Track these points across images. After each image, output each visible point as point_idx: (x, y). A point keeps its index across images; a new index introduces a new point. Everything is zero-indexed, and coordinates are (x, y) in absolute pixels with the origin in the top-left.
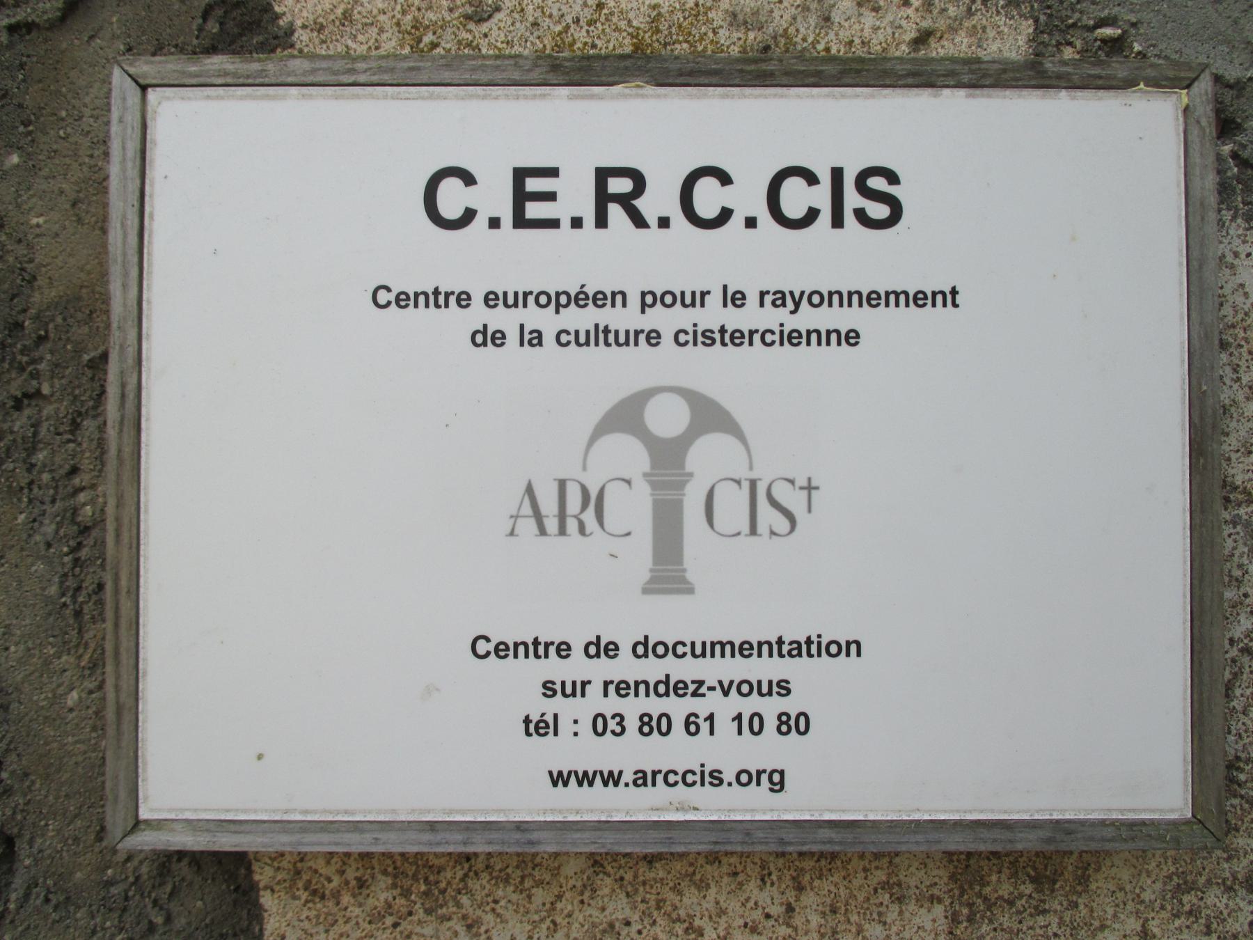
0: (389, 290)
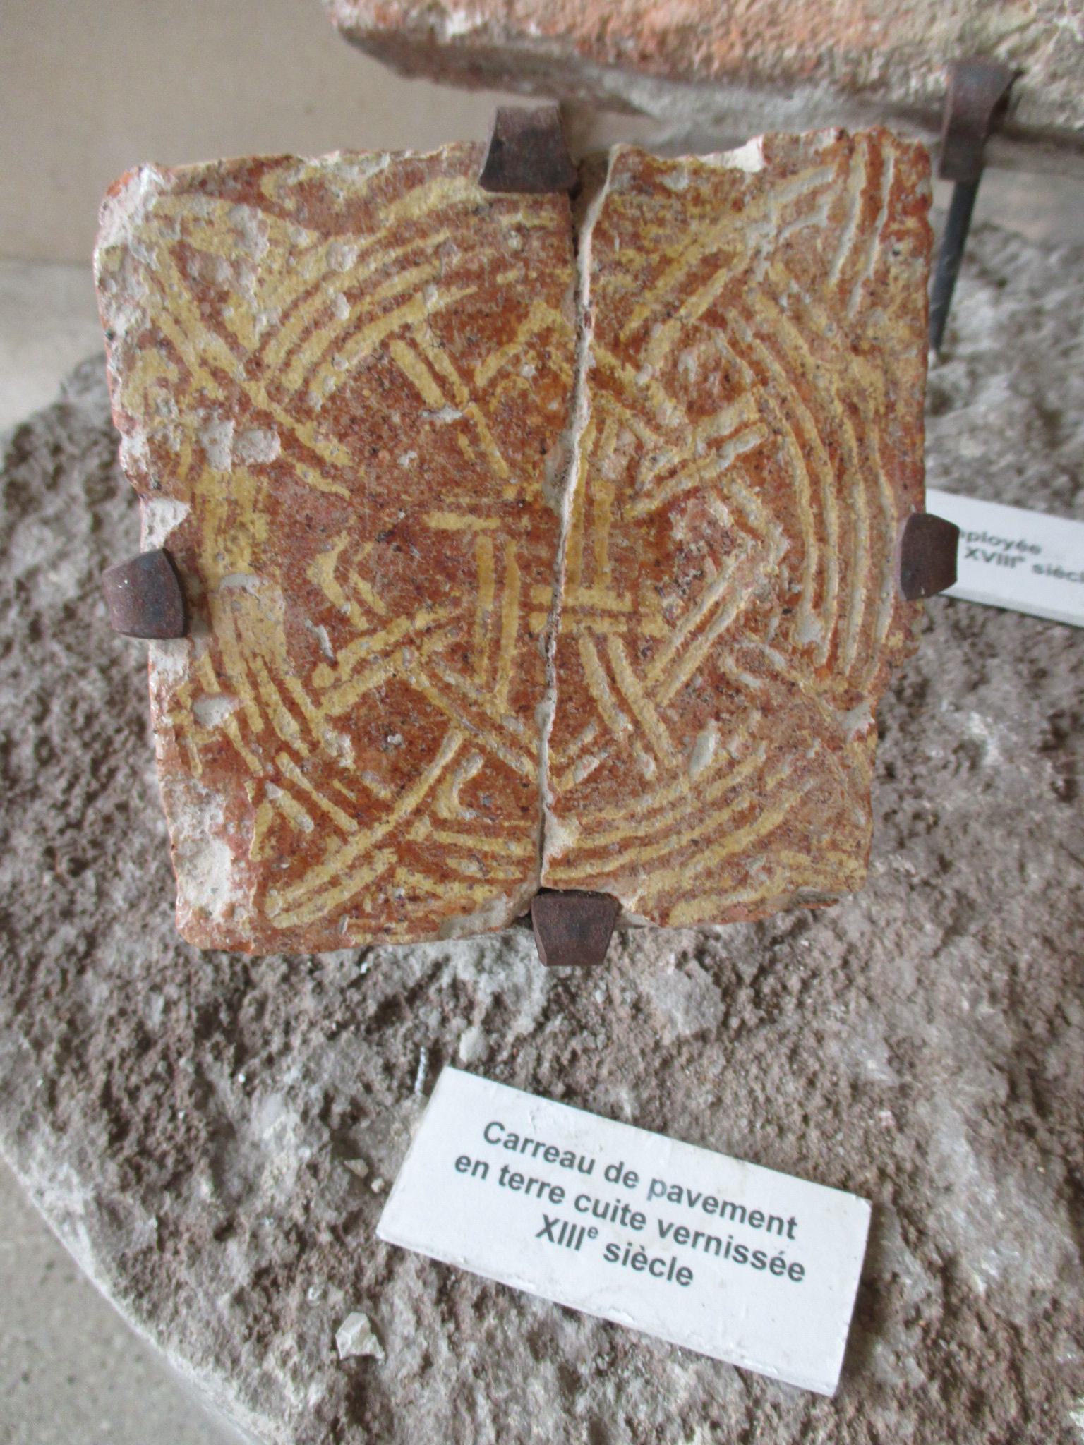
0: (502, 1128)
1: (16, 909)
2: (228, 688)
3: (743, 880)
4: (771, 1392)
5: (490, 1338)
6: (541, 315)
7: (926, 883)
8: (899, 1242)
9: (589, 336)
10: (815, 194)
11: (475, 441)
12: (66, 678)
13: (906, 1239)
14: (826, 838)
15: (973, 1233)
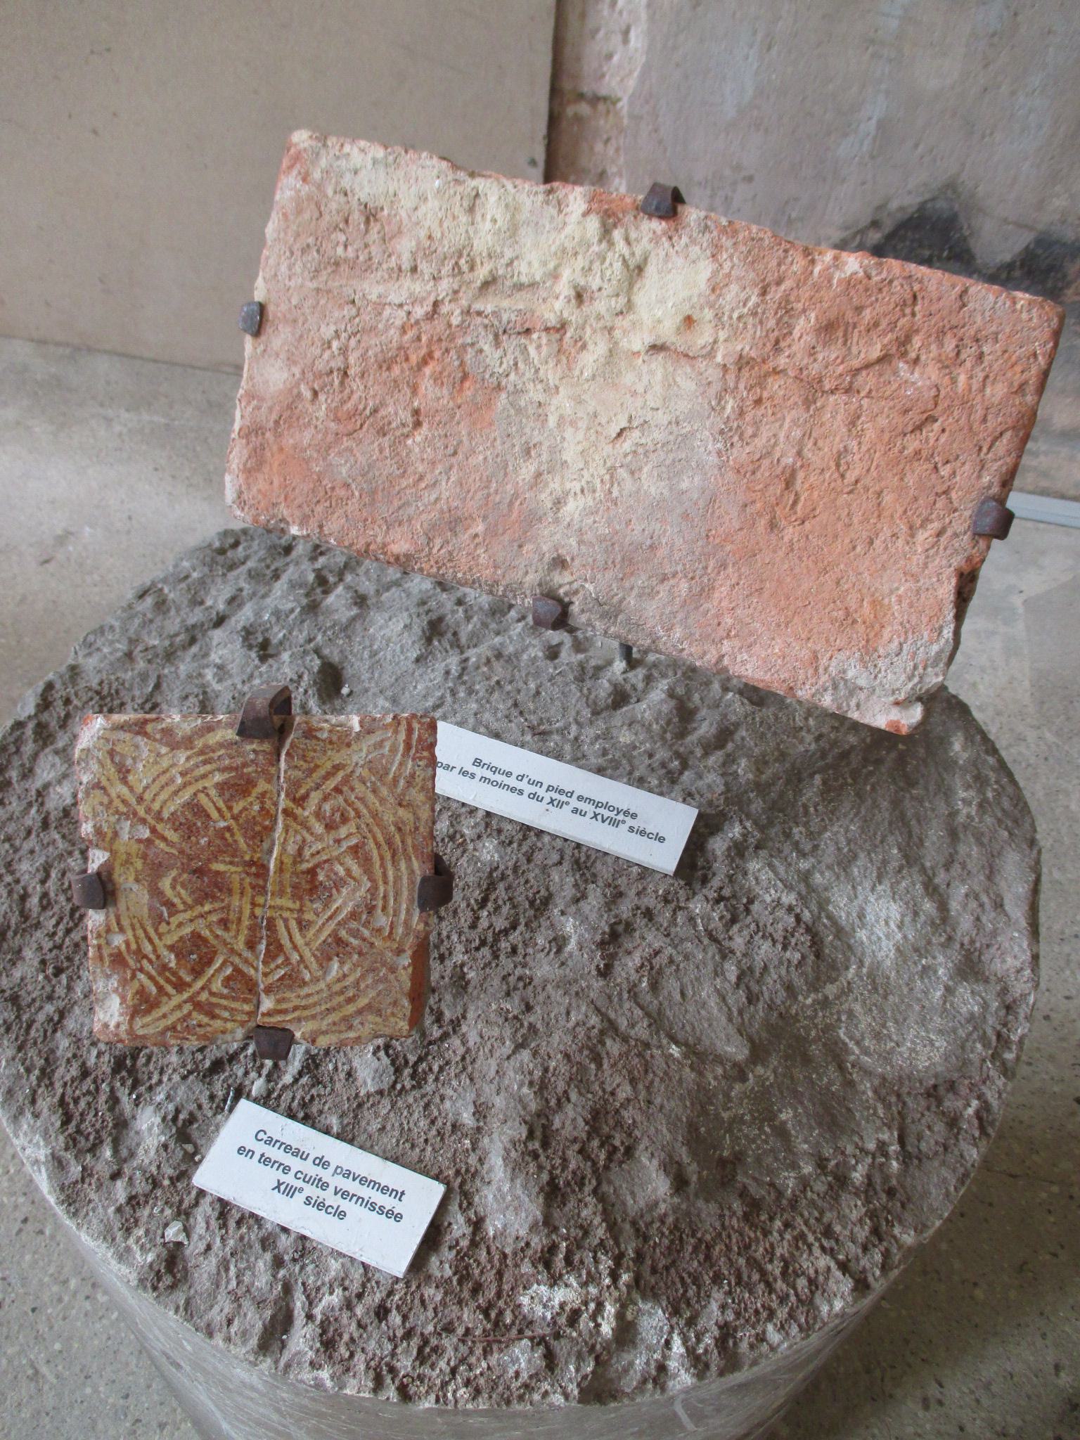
1: (22, 993)
2: (122, 930)
3: (350, 1027)
4: (377, 1275)
5: (242, 1238)
6: (262, 786)
7: (515, 1017)
8: (456, 1207)
9: (283, 795)
10: (382, 741)
11: (232, 835)
12: (61, 857)
13: (460, 1207)
14: (389, 1011)
15: (495, 1206)
